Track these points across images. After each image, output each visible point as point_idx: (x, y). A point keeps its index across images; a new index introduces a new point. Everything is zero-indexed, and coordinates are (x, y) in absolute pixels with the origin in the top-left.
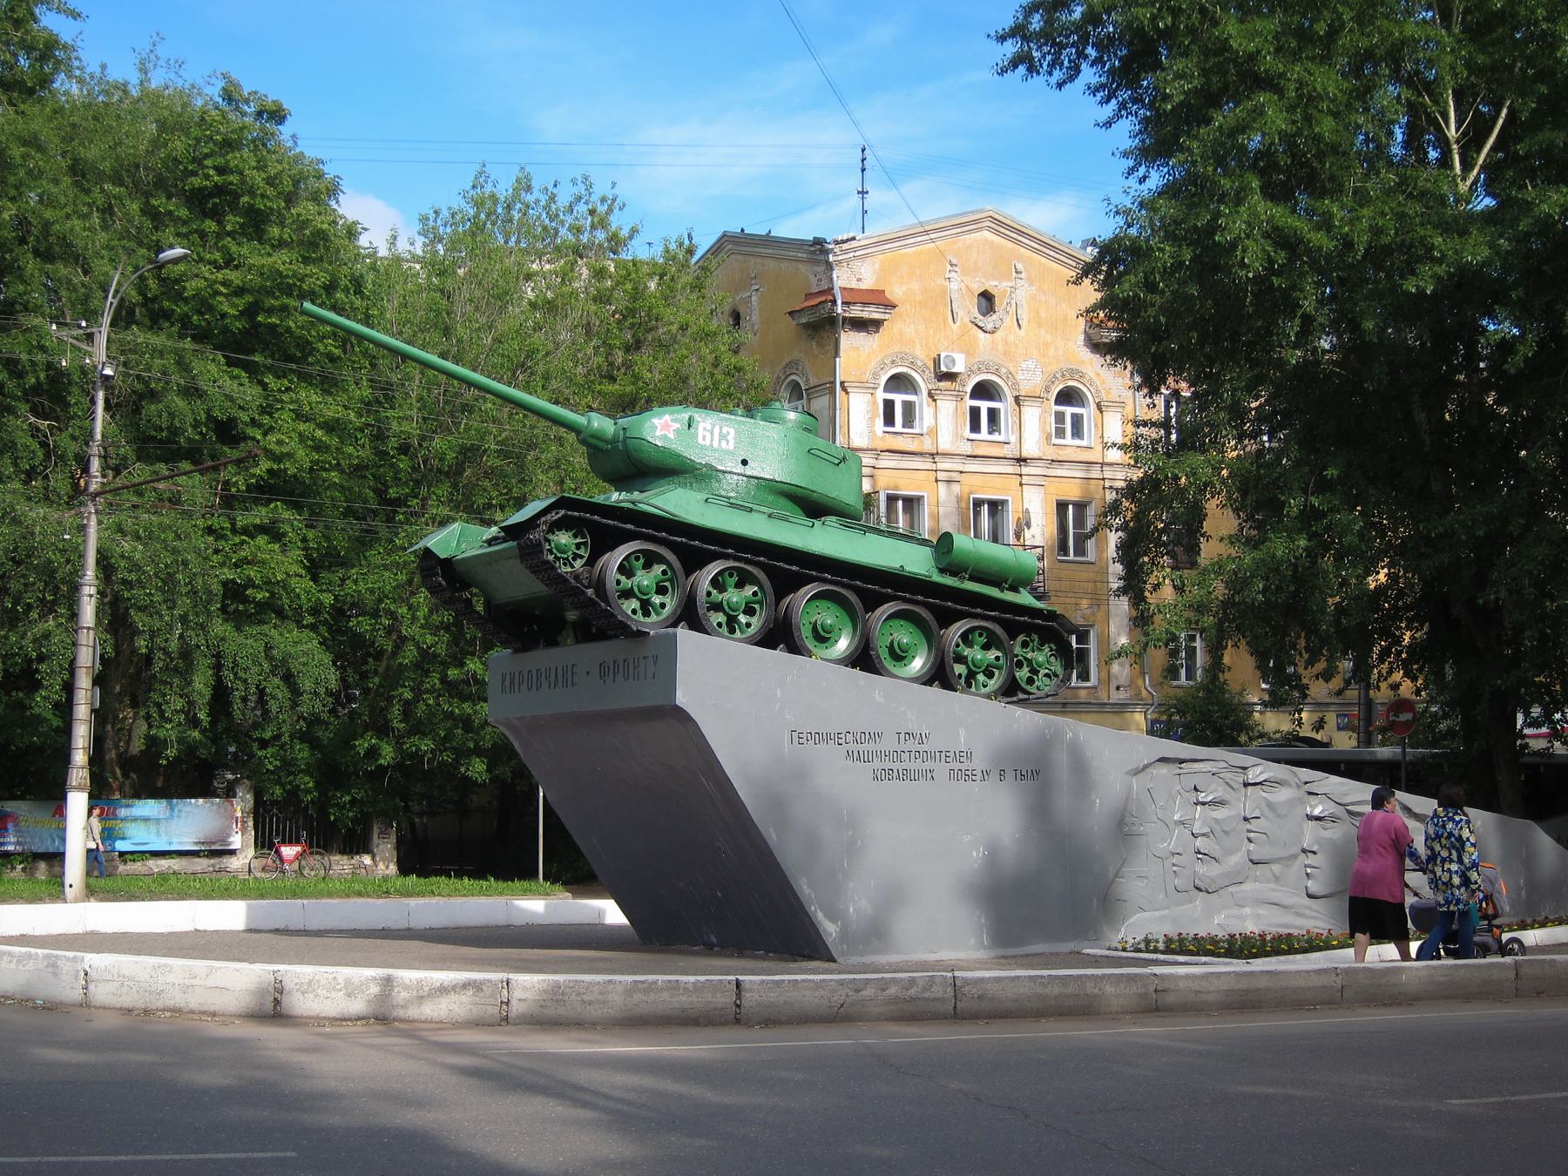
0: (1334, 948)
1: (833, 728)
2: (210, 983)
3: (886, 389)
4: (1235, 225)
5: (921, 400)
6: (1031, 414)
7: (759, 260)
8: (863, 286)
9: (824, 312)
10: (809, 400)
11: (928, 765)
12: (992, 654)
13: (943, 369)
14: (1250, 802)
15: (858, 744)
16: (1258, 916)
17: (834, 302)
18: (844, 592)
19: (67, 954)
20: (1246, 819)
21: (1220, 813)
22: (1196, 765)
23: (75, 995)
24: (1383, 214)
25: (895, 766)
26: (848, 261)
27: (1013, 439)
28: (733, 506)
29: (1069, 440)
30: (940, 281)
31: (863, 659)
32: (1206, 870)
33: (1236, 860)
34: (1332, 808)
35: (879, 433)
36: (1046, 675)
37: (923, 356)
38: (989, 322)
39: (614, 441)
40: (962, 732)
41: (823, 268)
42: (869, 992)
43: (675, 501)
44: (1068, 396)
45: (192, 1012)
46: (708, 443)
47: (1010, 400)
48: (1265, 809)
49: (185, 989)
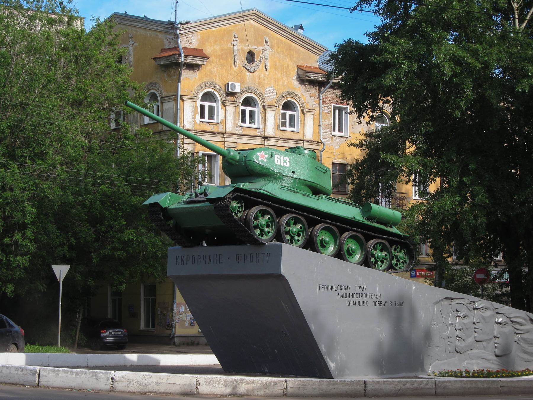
0: (519, 376)
1: (333, 284)
2: (169, 382)
3: (202, 100)
4: (439, 56)
5: (218, 106)
6: (271, 114)
7: (134, 29)
8: (192, 47)
9: (173, 60)
10: (162, 103)
11: (365, 300)
12: (384, 254)
13: (230, 90)
14: (475, 317)
15: (341, 291)
16: (478, 364)
17: (180, 55)
18: (333, 227)
19: (102, 371)
20: (474, 323)
21: (466, 321)
22: (457, 301)
23: (108, 387)
24: (500, 52)
25: (355, 299)
26: (186, 34)
27: (261, 127)
28: (290, 190)
29: (288, 128)
30: (229, 45)
31: (339, 255)
32: (460, 344)
33: (471, 340)
34: (506, 320)
35: (198, 122)
36: (402, 262)
37: (220, 83)
38: (252, 67)
39: (240, 161)
40: (377, 286)
41: (172, 37)
42: (408, 385)
43: (270, 188)
44: (288, 106)
45: (160, 393)
46: (279, 163)
47: (261, 107)
48: (481, 319)
49: (158, 384)
